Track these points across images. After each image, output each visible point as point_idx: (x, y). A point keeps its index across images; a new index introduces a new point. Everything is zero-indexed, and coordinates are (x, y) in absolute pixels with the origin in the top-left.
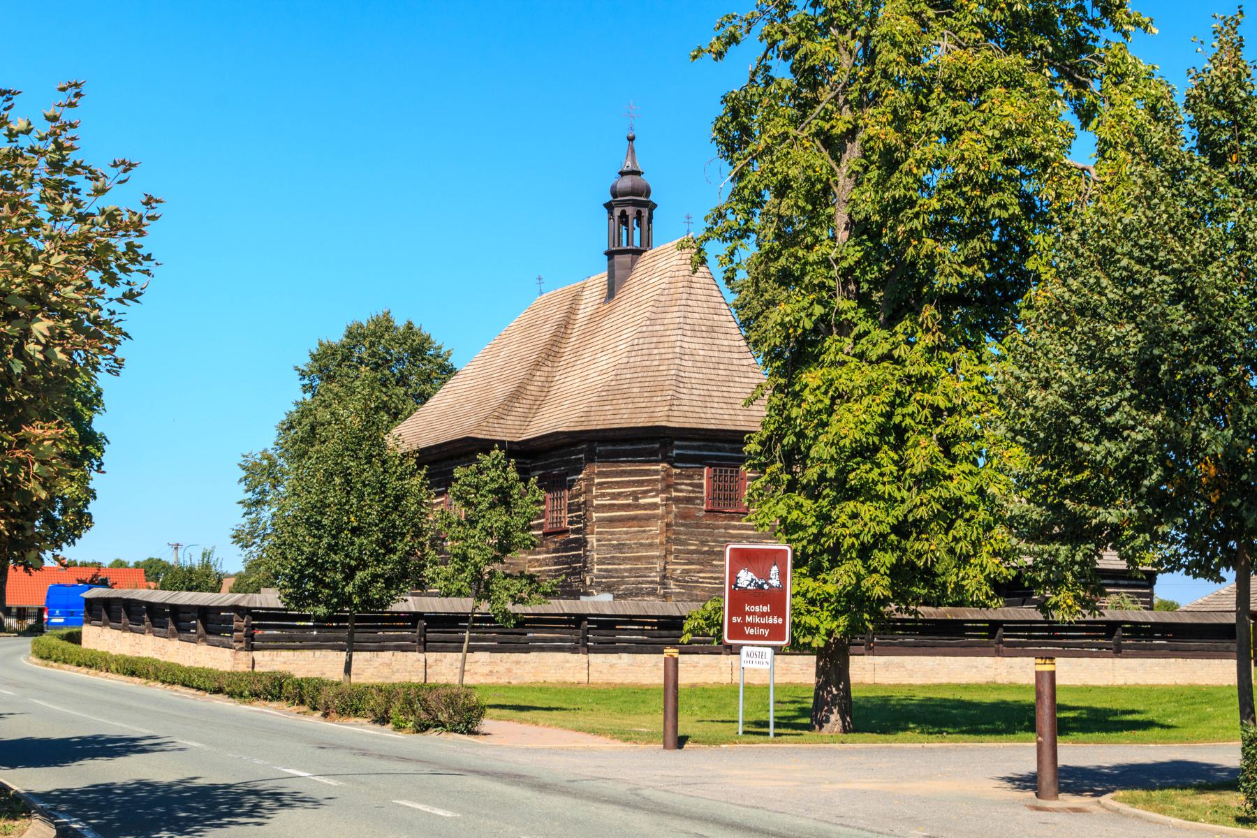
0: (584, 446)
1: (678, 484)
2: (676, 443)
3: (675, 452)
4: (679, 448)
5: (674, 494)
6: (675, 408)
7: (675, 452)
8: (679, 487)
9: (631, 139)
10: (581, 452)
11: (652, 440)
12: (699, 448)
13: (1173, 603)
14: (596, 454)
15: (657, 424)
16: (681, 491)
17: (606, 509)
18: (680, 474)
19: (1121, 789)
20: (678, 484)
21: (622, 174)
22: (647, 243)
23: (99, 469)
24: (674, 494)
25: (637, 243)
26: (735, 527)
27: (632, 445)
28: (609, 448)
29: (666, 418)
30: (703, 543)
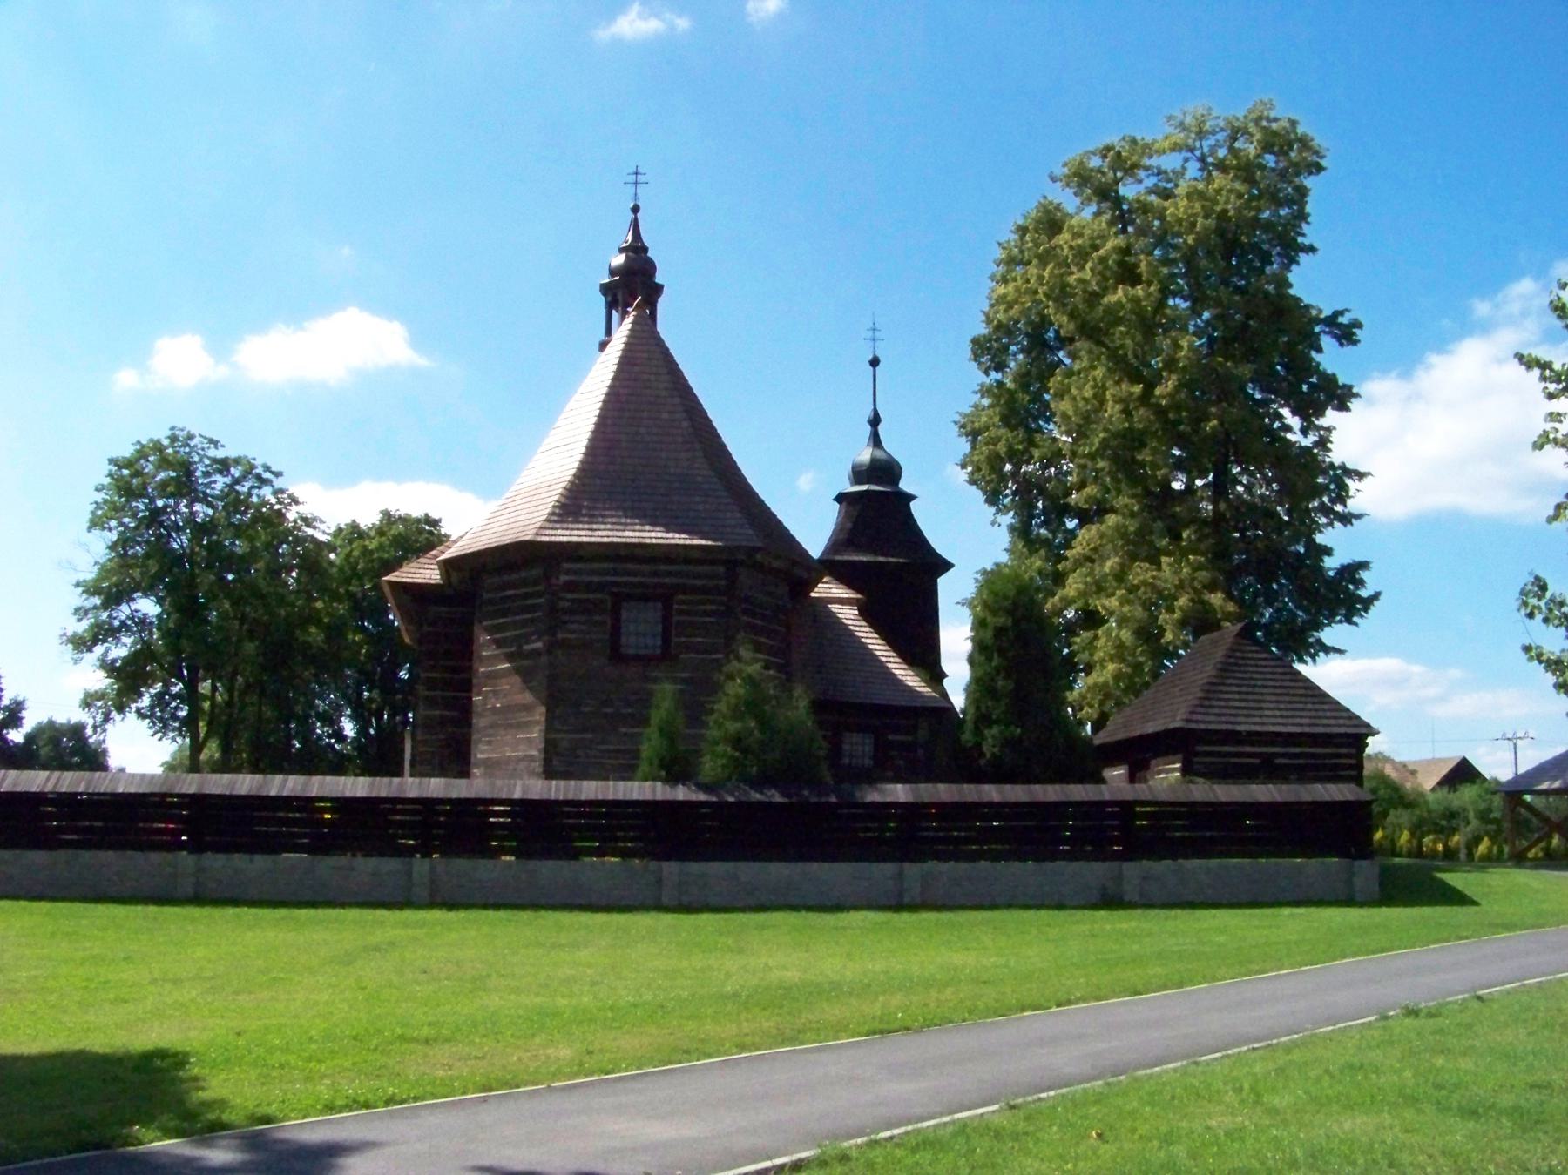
2: (566, 566)
4: (567, 572)
9: (636, 209)
16: (574, 632)
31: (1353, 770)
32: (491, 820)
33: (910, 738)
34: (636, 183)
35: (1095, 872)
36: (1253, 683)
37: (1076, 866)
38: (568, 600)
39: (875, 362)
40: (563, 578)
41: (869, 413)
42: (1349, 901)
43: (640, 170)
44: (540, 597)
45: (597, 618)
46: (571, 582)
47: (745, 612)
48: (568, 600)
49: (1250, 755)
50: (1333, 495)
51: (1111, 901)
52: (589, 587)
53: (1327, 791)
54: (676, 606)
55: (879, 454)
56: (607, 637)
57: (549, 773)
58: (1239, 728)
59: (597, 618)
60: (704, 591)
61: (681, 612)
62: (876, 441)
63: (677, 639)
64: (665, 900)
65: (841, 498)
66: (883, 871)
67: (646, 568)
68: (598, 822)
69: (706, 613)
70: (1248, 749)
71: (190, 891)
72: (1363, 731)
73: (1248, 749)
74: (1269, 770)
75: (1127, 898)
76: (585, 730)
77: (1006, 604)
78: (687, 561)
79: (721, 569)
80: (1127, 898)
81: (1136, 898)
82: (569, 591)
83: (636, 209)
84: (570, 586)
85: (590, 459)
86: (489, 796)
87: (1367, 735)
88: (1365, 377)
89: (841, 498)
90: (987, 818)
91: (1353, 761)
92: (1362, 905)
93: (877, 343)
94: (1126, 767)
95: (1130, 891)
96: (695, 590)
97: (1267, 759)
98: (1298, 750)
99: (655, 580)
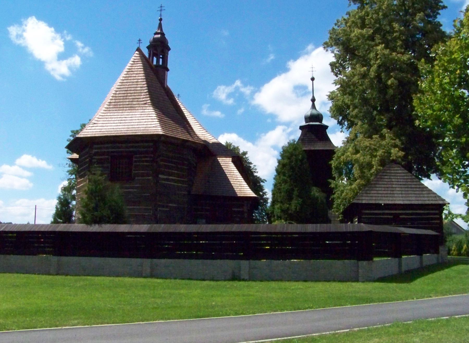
4: (96, 149)
9: (161, 20)
21: (156, 33)
31: (438, 220)
34: (161, 10)
36: (392, 183)
39: (313, 79)
40: (95, 151)
41: (311, 97)
42: (49, 274)
43: (162, 6)
46: (97, 152)
47: (162, 160)
49: (388, 214)
50: (339, 73)
51: (235, 277)
52: (103, 154)
54: (134, 159)
55: (314, 112)
56: (109, 172)
58: (380, 202)
61: (136, 162)
62: (314, 107)
63: (133, 172)
65: (301, 128)
66: (147, 262)
67: (124, 145)
69: (147, 161)
72: (441, 202)
75: (242, 277)
77: (287, 154)
78: (137, 142)
80: (242, 277)
81: (247, 277)
83: (161, 20)
84: (96, 154)
85: (302, 137)
89: (301, 128)
90: (198, 239)
91: (438, 216)
92: (145, 277)
93: (313, 72)
95: (244, 274)
96: (141, 153)
97: (396, 216)
98: (411, 212)
99: (127, 150)
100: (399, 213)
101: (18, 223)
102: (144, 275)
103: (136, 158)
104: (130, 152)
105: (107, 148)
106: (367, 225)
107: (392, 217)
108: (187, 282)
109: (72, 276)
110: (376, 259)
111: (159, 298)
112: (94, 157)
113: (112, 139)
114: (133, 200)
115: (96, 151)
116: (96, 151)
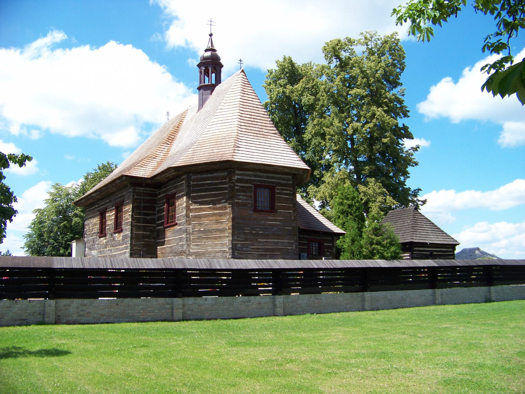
0: (185, 176)
1: (239, 195)
2: (237, 172)
3: (236, 177)
4: (238, 175)
5: (236, 201)
6: (236, 151)
7: (236, 177)
8: (239, 197)
9: (211, 35)
10: (183, 180)
11: (223, 170)
12: (249, 175)
13: (11, 194)
14: (191, 180)
15: (226, 159)
16: (240, 199)
17: (198, 210)
18: (239, 189)
19: (284, 258)
20: (239, 195)
21: (206, 50)
22: (218, 81)
23: (16, 201)
24: (236, 201)
25: (213, 82)
26: (270, 220)
27: (212, 174)
28: (199, 176)
29: (232, 151)
30: (253, 229)
32: (302, 272)
33: (331, 245)
35: (483, 290)
37: (477, 288)
38: (161, 203)
44: (226, 184)
45: (249, 194)
48: (161, 203)
51: (488, 300)
52: (247, 181)
53: (316, 263)
57: (234, 257)
58: (427, 242)
59: (249, 194)
60: (285, 185)
64: (366, 308)
68: (166, 271)
70: (427, 249)
71: (181, 316)
72: (454, 243)
73: (427, 249)
74: (431, 256)
76: (246, 240)
79: (290, 177)
82: (240, 183)
84: (239, 181)
86: (5, 266)
87: (456, 245)
88: (417, 138)
91: (452, 253)
94: (410, 253)
97: (432, 252)
100: (433, 251)
101: (503, 257)
102: (437, 303)
103: (278, 189)
104: (272, 183)
105: (249, 175)
106: (419, 261)
107: (429, 253)
108: (375, 312)
109: (414, 307)
110: (292, 294)
111: (240, 343)
112: (236, 184)
113: (287, 171)
114: (277, 233)
115: (239, 177)
116: (239, 177)
